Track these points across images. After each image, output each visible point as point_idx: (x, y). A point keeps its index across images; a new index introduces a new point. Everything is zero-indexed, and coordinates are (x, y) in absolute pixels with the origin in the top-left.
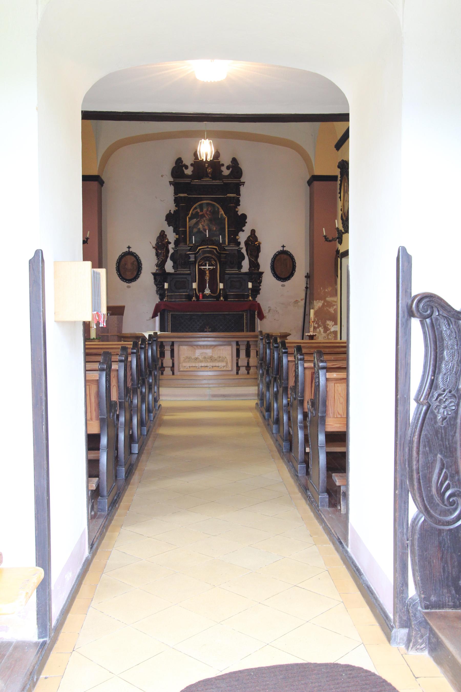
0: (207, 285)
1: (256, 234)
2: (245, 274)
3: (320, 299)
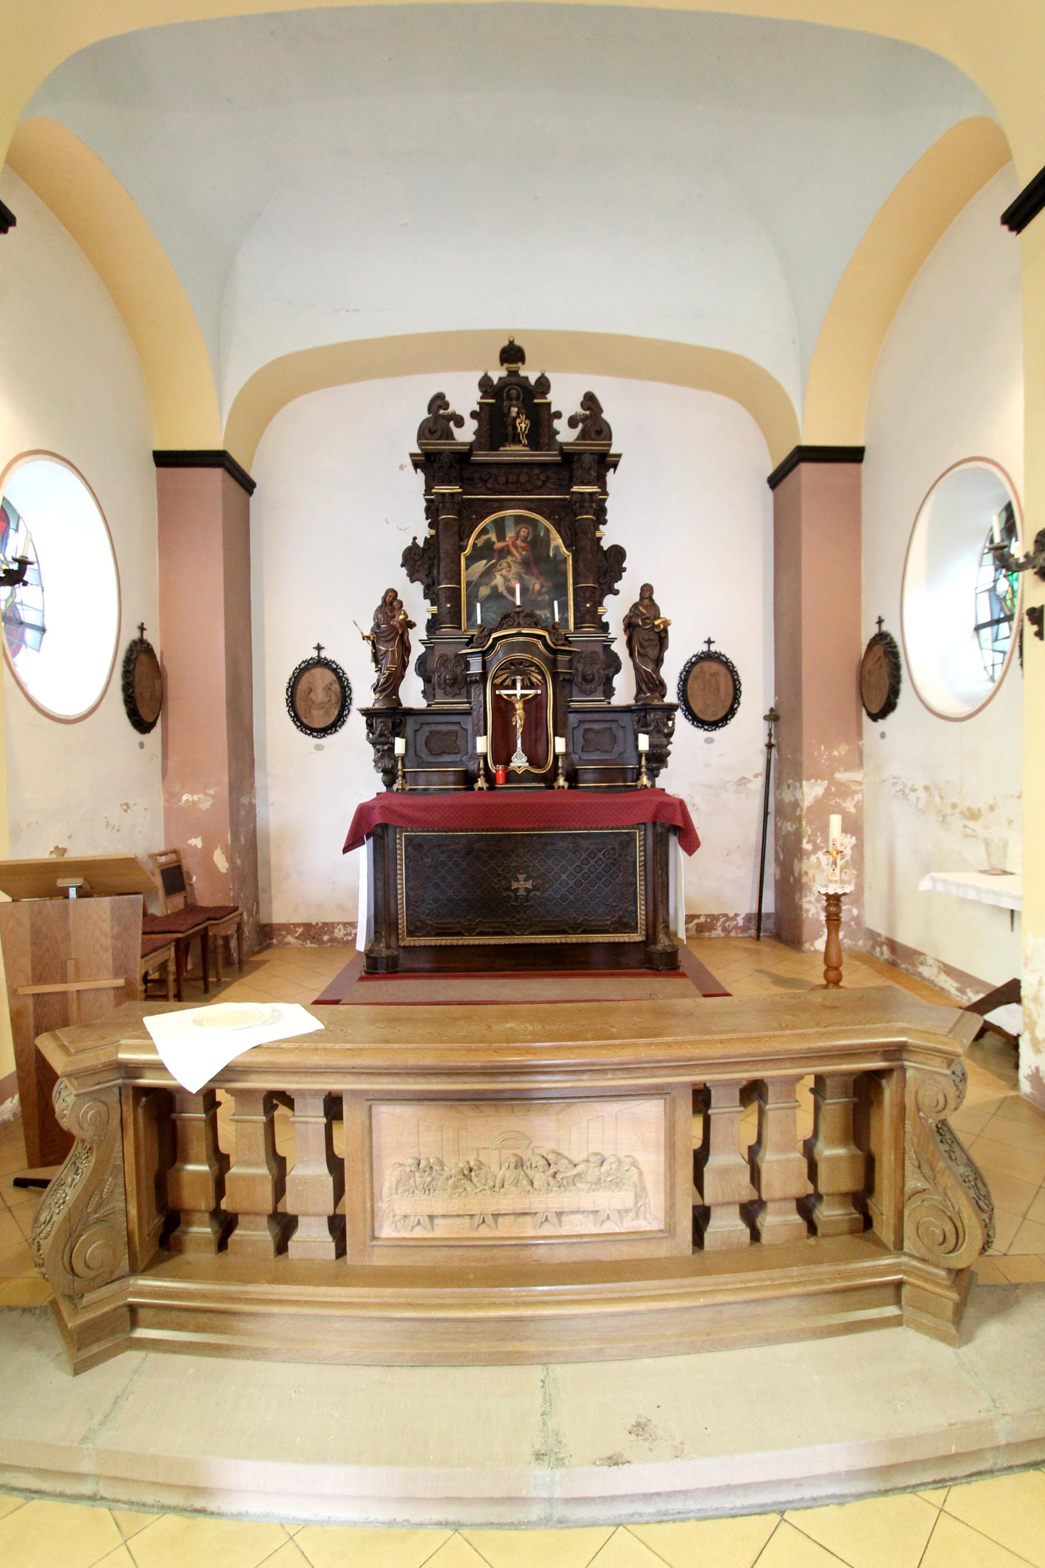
0: (519, 742)
2: (627, 710)
3: (818, 776)
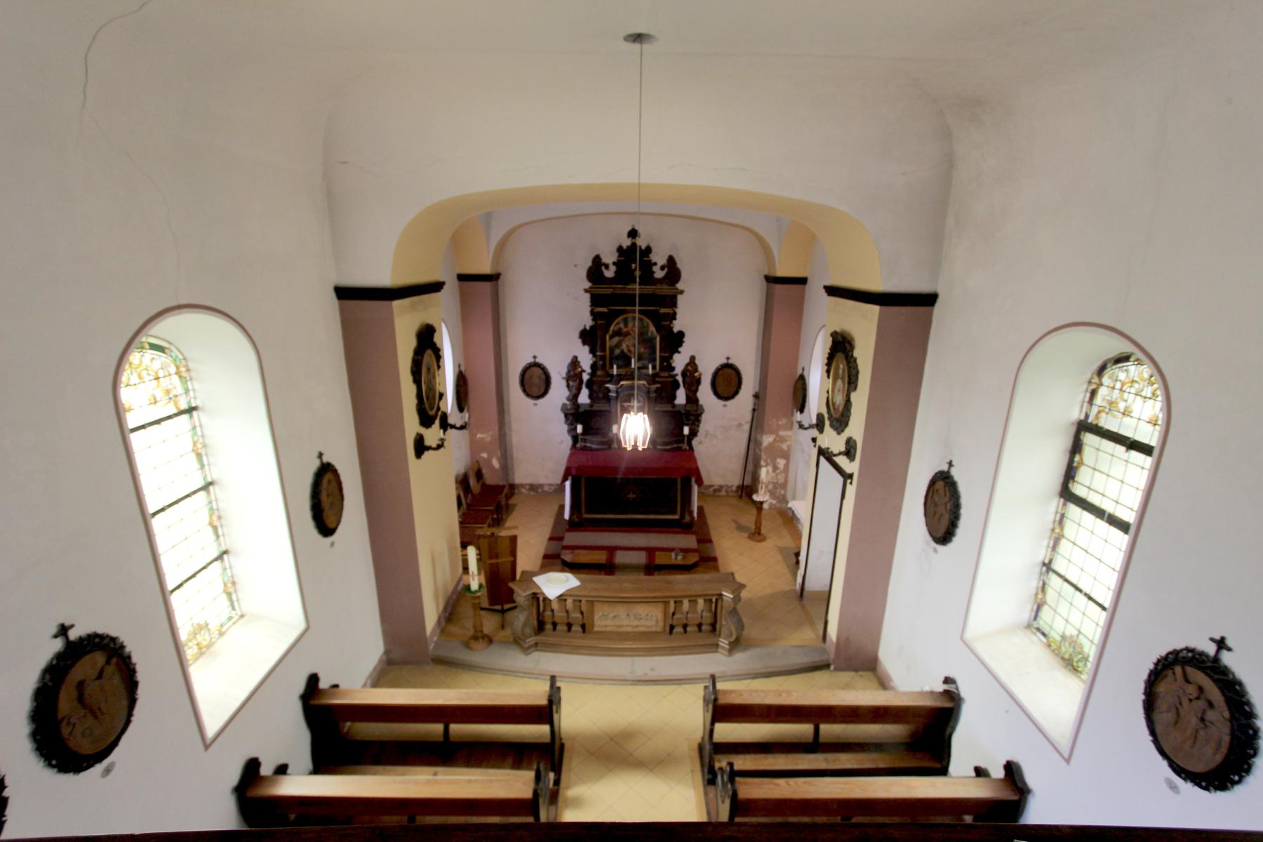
1: (697, 362)
3: (771, 432)
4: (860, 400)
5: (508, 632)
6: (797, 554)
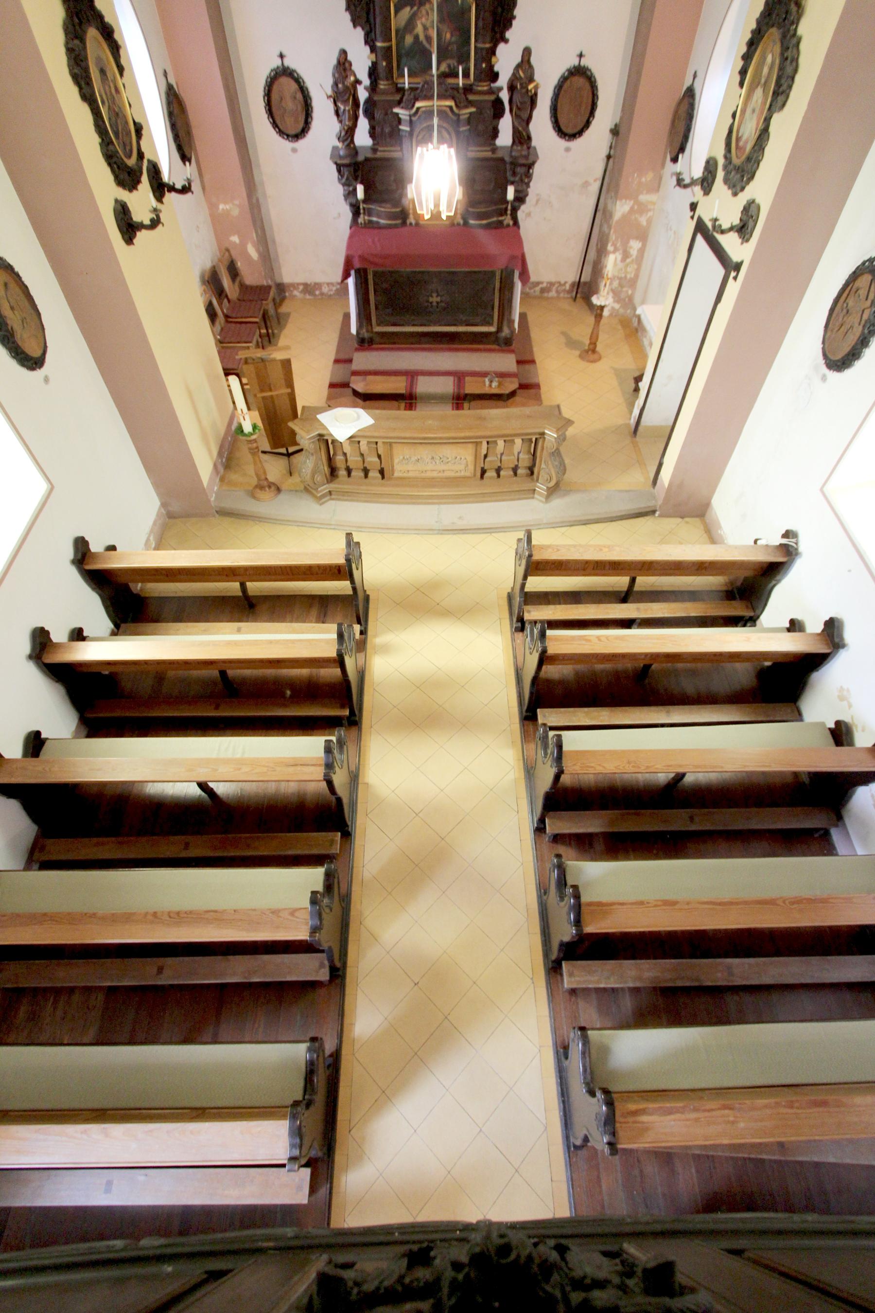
3: (627, 197)
4: (786, 126)
5: (296, 479)
6: (638, 379)
